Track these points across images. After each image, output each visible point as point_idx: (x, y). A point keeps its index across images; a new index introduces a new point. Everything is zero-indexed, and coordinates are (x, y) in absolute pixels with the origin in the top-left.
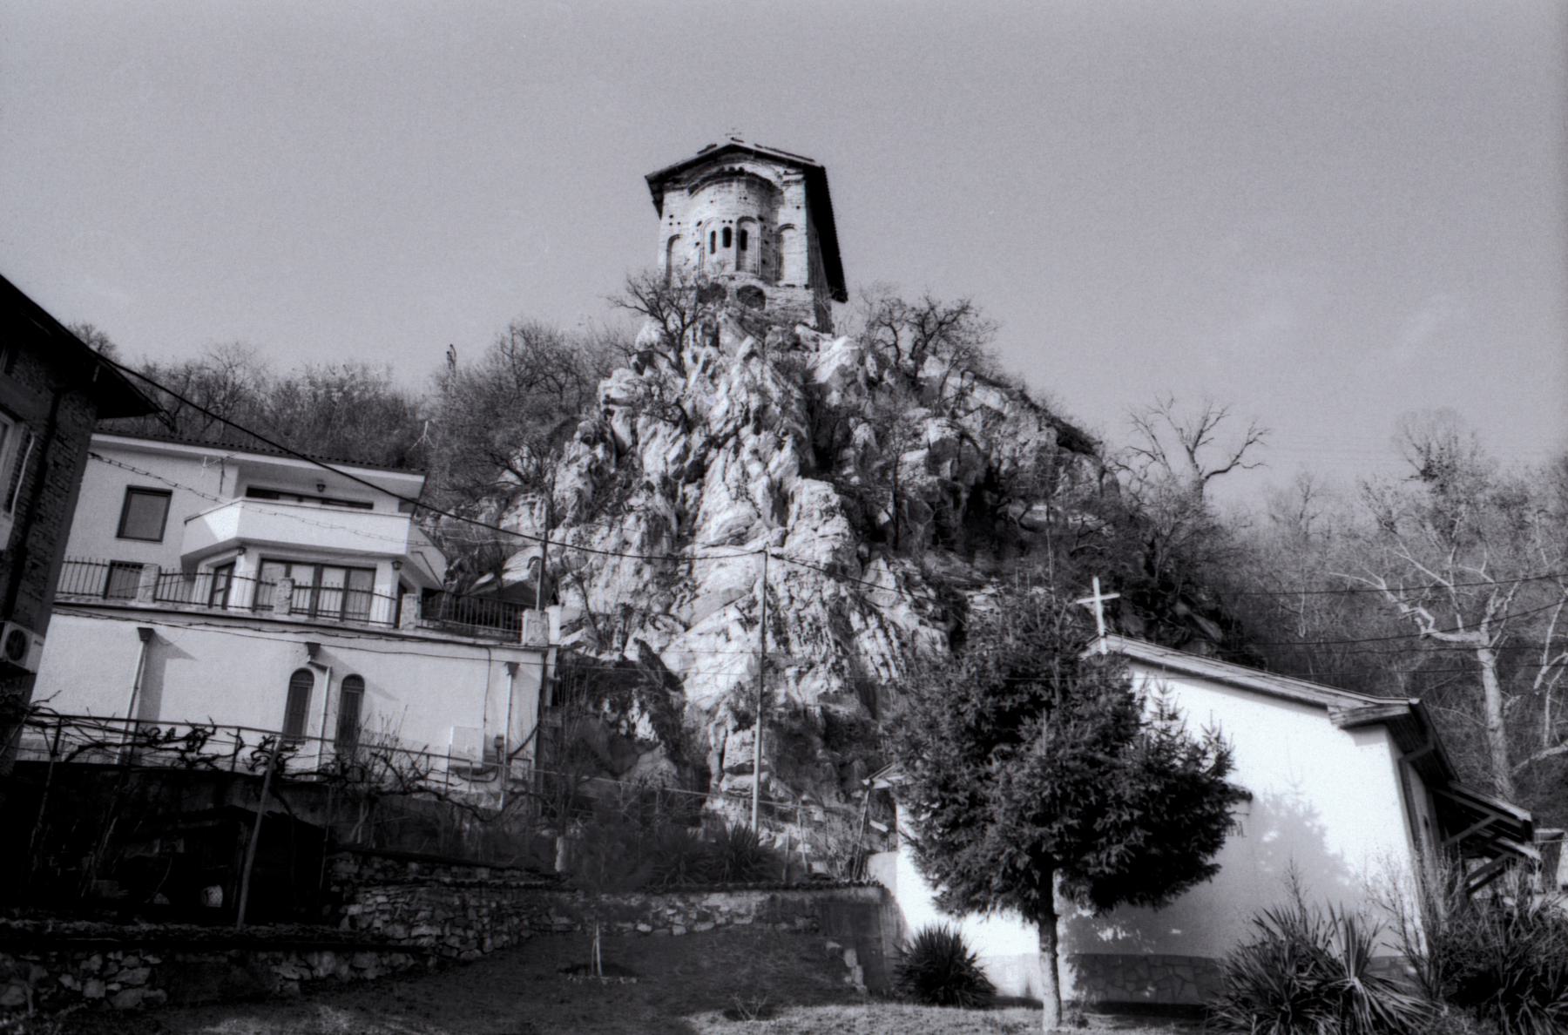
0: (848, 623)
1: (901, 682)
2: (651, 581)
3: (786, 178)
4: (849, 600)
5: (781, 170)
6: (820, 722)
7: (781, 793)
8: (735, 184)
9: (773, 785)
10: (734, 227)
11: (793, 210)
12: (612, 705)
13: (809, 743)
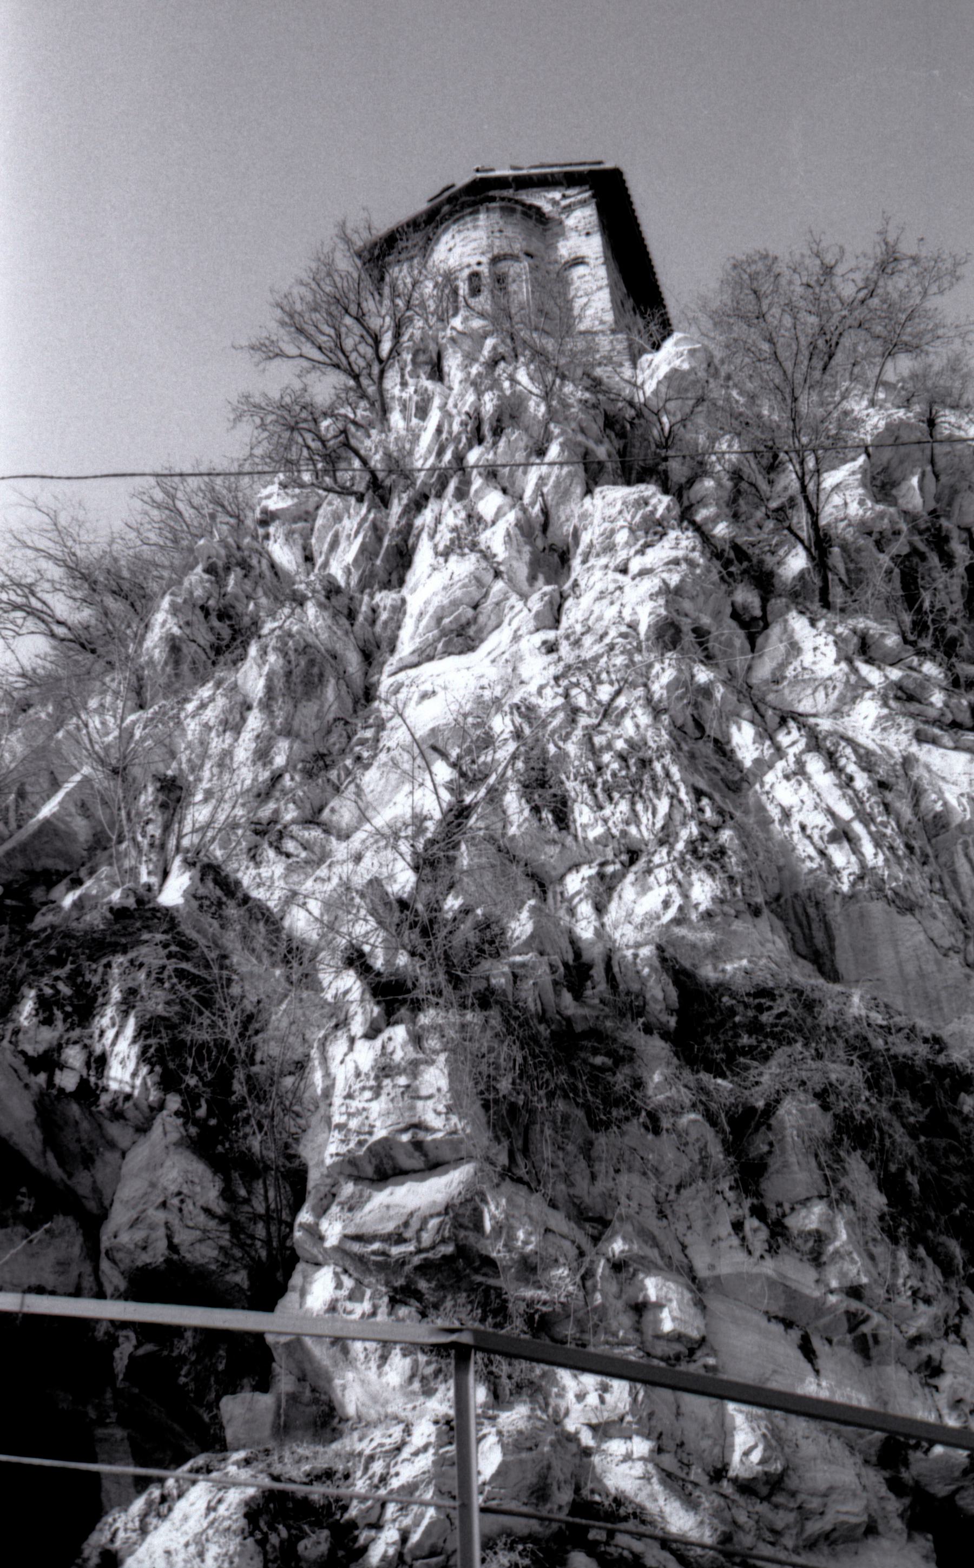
0: (723, 749)
1: (900, 878)
2: (290, 765)
3: (564, 203)
4: (719, 692)
5: (557, 195)
6: (659, 992)
7: (525, 1238)
8: (482, 216)
9: (492, 1213)
10: (484, 270)
11: (581, 236)
12: (45, 1006)
13: (625, 1056)
